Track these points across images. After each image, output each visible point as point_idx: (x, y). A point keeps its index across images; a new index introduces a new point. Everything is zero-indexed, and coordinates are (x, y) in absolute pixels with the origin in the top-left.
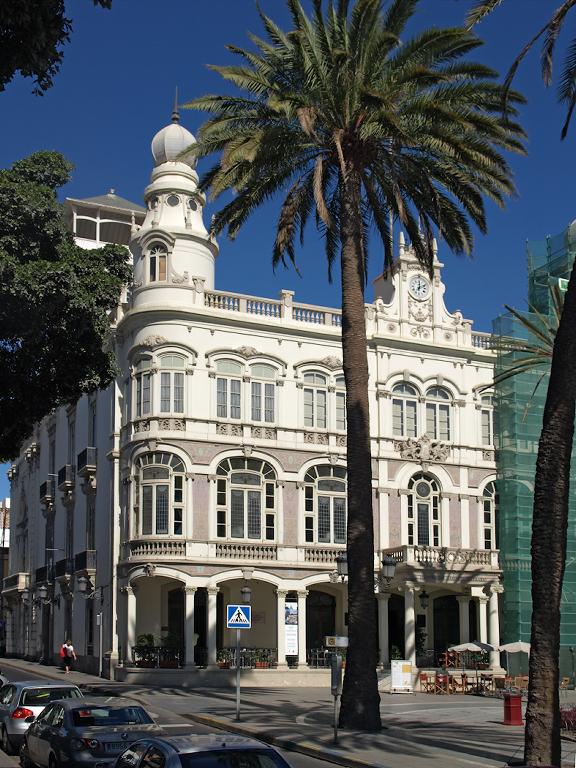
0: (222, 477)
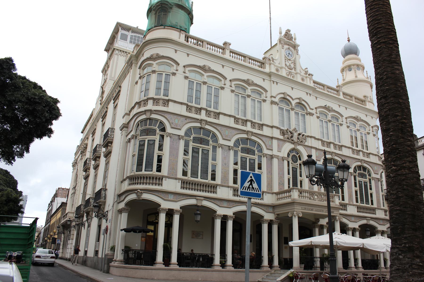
0: (187, 138)
